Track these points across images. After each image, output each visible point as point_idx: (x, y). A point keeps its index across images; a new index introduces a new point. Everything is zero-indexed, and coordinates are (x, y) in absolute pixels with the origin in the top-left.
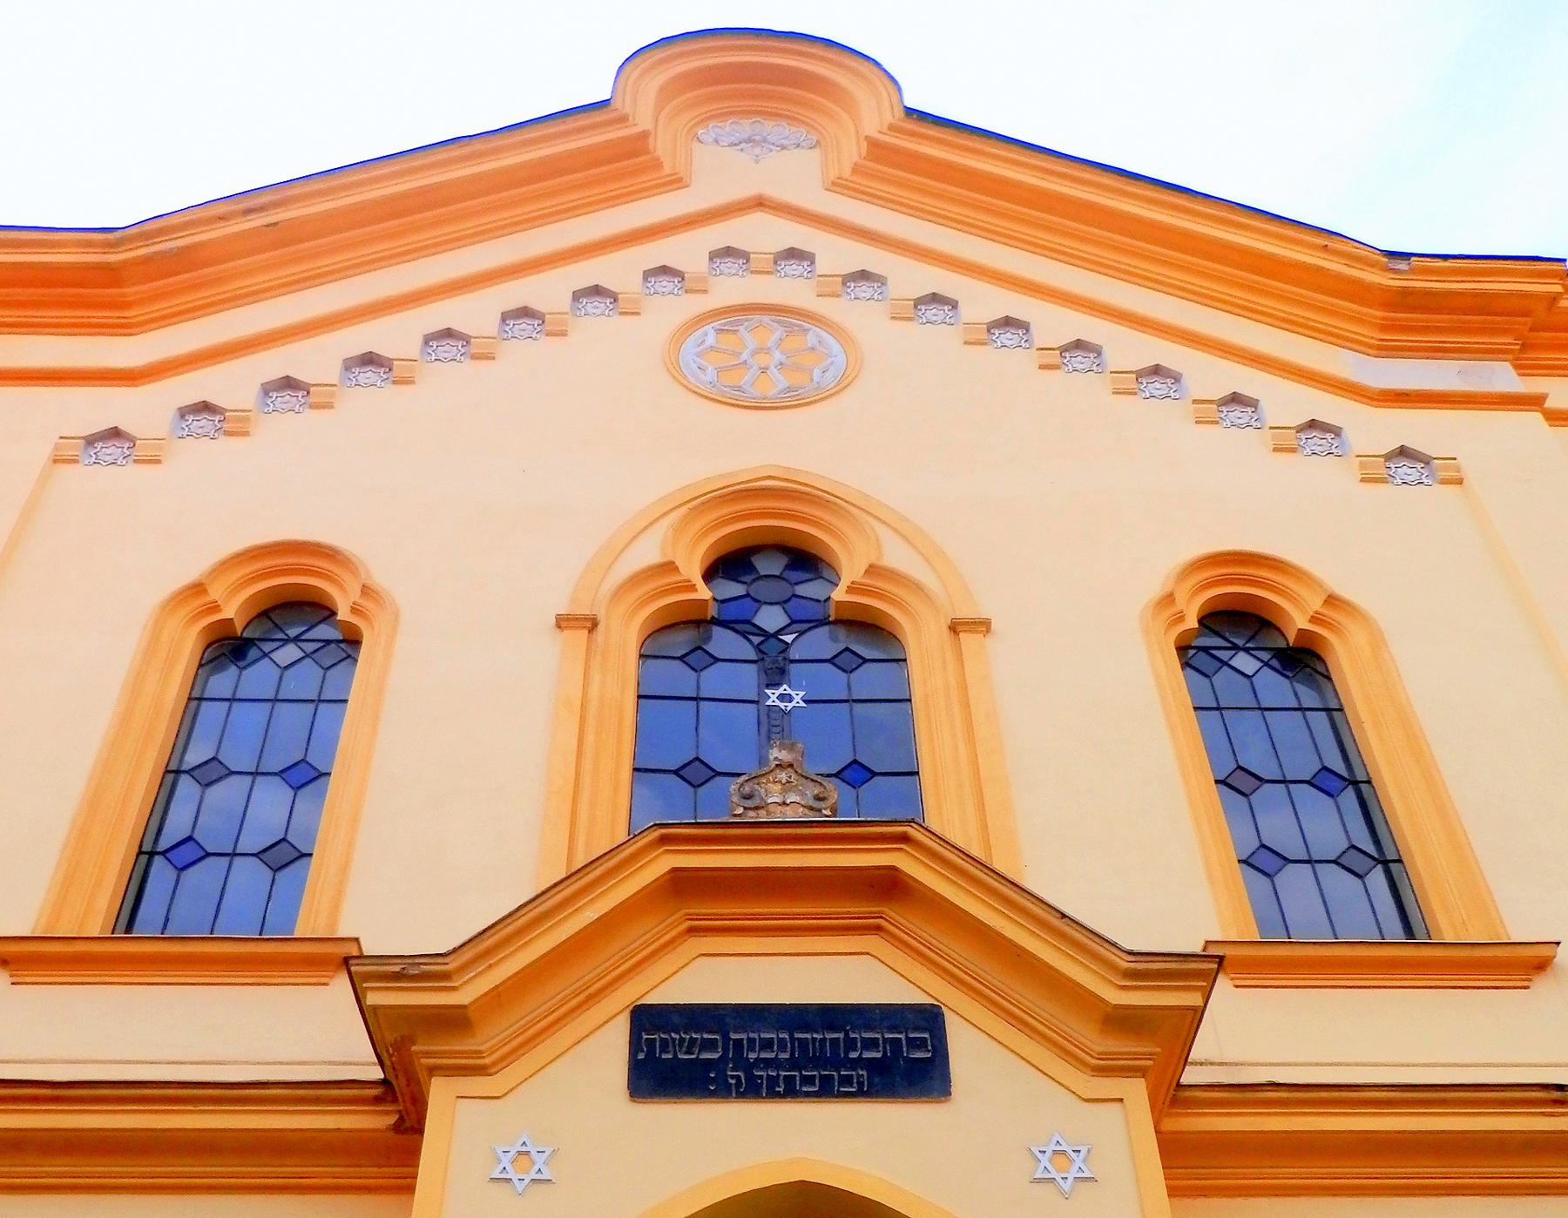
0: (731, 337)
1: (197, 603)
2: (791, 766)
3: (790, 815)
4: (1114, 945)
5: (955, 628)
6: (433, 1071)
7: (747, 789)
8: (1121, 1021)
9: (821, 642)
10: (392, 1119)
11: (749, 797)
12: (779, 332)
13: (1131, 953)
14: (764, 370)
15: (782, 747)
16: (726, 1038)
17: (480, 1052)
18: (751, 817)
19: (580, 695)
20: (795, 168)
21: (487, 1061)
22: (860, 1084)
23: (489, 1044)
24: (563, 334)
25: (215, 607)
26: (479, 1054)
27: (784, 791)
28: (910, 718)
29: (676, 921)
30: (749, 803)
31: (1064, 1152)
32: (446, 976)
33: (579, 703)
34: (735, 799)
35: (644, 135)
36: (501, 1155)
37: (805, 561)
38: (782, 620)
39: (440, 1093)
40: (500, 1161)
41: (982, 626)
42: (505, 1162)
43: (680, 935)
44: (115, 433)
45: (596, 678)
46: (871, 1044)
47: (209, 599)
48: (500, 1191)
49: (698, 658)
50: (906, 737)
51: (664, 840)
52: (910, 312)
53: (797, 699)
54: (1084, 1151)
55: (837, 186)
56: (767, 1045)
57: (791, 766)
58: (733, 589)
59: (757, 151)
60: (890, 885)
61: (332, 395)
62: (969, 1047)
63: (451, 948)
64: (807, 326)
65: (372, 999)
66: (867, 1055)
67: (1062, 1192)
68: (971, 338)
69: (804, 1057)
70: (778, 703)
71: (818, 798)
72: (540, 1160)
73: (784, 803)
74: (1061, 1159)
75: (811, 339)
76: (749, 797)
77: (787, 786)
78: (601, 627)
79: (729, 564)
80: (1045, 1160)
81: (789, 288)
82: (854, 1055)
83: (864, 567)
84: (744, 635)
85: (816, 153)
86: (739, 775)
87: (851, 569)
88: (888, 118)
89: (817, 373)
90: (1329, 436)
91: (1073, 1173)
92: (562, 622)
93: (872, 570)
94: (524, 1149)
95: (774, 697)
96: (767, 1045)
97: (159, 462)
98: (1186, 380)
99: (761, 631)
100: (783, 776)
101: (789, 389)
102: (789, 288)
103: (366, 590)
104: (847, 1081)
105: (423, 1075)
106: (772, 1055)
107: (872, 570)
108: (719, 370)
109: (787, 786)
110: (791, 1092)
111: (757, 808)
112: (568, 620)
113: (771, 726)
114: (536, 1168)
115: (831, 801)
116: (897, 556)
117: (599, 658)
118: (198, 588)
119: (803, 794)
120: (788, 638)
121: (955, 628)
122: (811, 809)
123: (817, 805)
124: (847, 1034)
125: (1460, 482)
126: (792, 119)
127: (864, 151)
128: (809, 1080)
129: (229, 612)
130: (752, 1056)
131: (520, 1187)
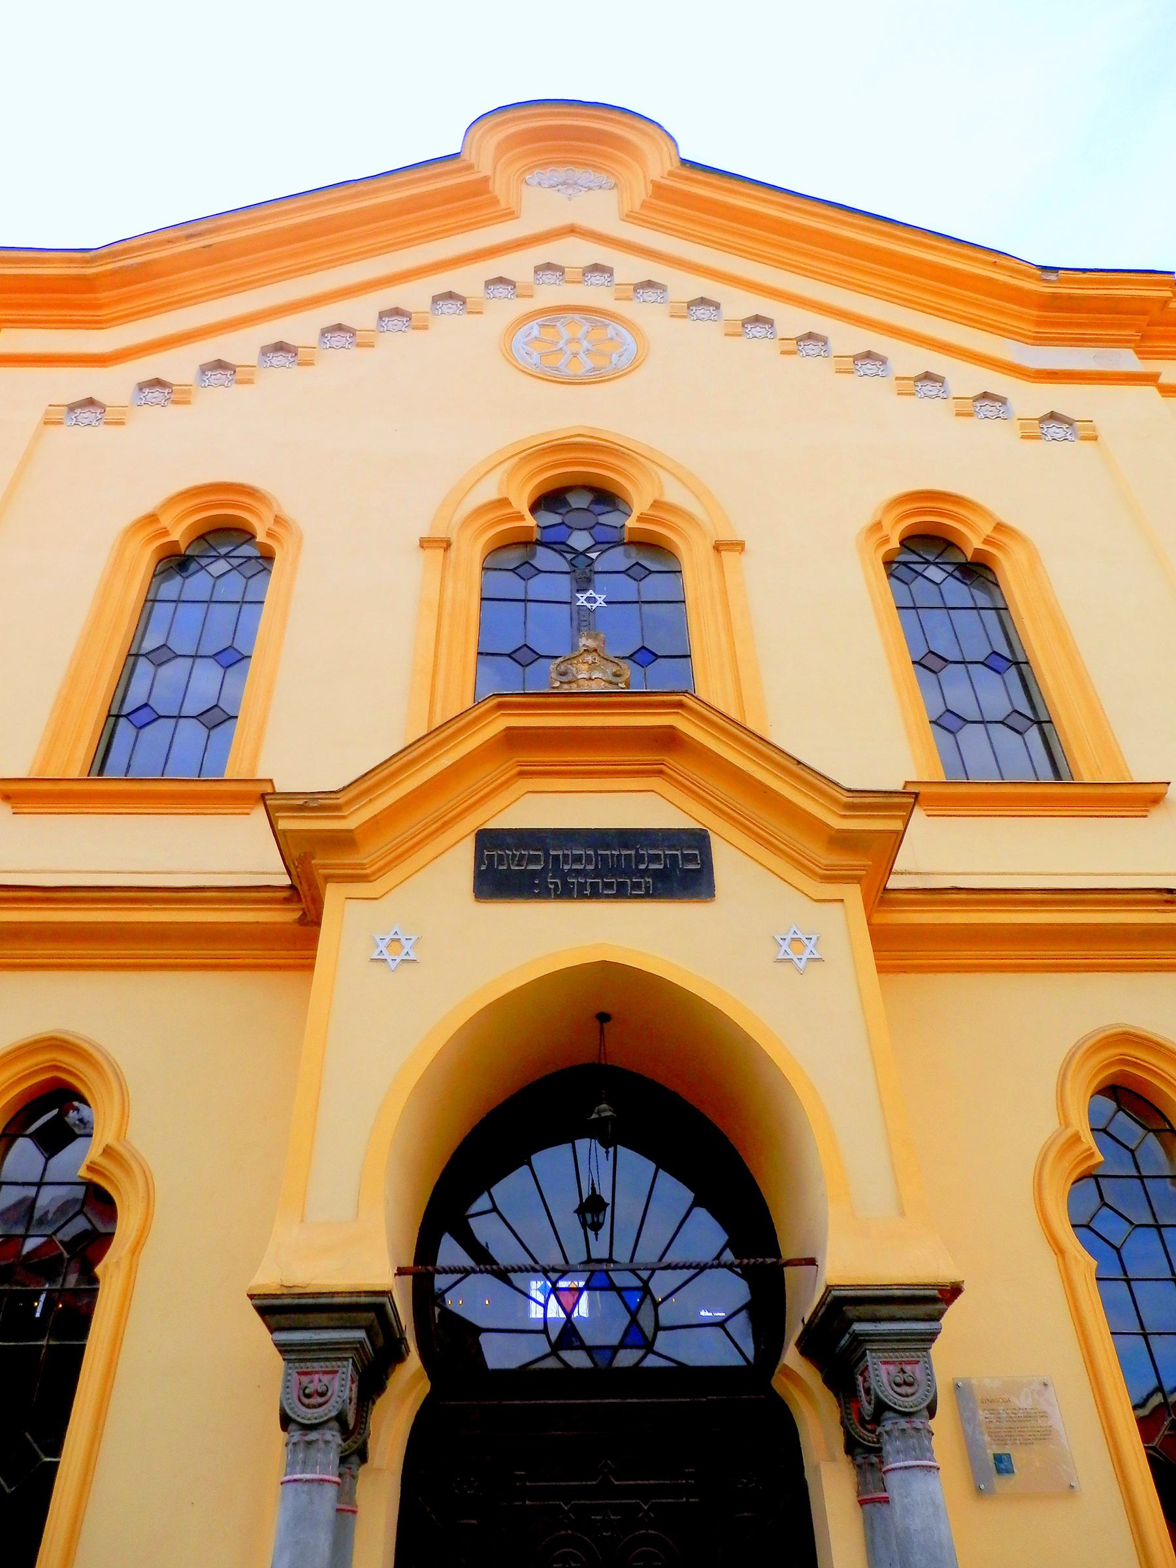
0: (551, 330)
1: (152, 529)
2: (595, 650)
3: (595, 687)
4: (837, 784)
5: (718, 548)
6: (327, 878)
7: (563, 668)
8: (842, 841)
9: (617, 558)
10: (297, 915)
11: (564, 674)
12: (587, 326)
13: (849, 791)
14: (575, 355)
15: (589, 637)
16: (547, 854)
18: (566, 688)
19: (437, 597)
20: (598, 204)
21: (368, 871)
22: (647, 888)
23: (369, 859)
24: (425, 328)
25: (165, 532)
27: (590, 670)
30: (564, 679)
31: (799, 940)
32: (337, 808)
34: (554, 675)
35: (486, 180)
37: (606, 497)
39: (333, 895)
40: (378, 946)
41: (738, 546)
42: (382, 947)
44: (90, 402)
45: (450, 585)
46: (655, 858)
47: (160, 526)
48: (378, 968)
51: (500, 706)
52: (684, 312)
53: (600, 600)
54: (814, 938)
55: (630, 217)
56: (578, 859)
57: (595, 650)
59: (570, 191)
60: (669, 740)
61: (253, 373)
62: (728, 860)
64: (607, 322)
65: (282, 825)
67: (798, 969)
68: (730, 331)
69: (605, 868)
70: (585, 603)
71: (616, 675)
72: (408, 946)
74: (796, 945)
75: (610, 332)
76: (564, 674)
77: (592, 666)
78: (454, 547)
80: (785, 945)
81: (594, 294)
82: (642, 867)
83: (650, 502)
84: (560, 553)
85: (614, 192)
87: (640, 504)
88: (668, 167)
89: (615, 357)
90: (997, 404)
91: (807, 955)
92: (425, 543)
93: (656, 504)
94: (396, 937)
95: (582, 600)
96: (578, 859)
97: (123, 423)
98: (891, 363)
99: (573, 550)
100: (589, 658)
101: (594, 369)
102: (594, 294)
103: (278, 520)
104: (637, 886)
105: (320, 881)
107: (656, 504)
108: (542, 355)
110: (595, 894)
111: (570, 682)
113: (580, 621)
115: (625, 677)
116: (674, 494)
118: (152, 518)
119: (604, 672)
121: (718, 548)
122: (611, 683)
123: (615, 680)
125: (1095, 438)
126: (596, 167)
127: (650, 193)
128: (608, 886)
129: (176, 535)
130: (566, 867)
131: (393, 965)
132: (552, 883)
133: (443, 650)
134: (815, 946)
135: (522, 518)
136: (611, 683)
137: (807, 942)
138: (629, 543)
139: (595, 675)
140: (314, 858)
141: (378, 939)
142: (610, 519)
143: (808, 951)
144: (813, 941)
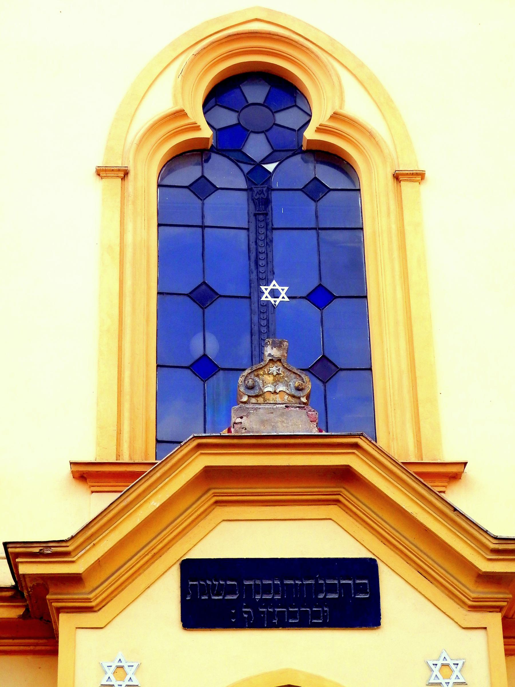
2: (279, 360)
4: (486, 532)
5: (397, 177)
6: (59, 610)
7: (250, 383)
10: (20, 612)
11: (252, 388)
13: (496, 538)
15: (274, 345)
16: (241, 584)
17: (90, 599)
19: (118, 241)
21: (93, 604)
22: (325, 618)
23: (94, 594)
26: (88, 600)
27: (276, 382)
28: (361, 242)
29: (209, 499)
30: (252, 393)
31: (448, 665)
32: (66, 554)
33: (118, 249)
34: (242, 389)
36: (107, 669)
37: (285, 90)
38: (266, 150)
39: (65, 624)
40: (106, 673)
41: (418, 176)
42: (110, 674)
43: (209, 507)
45: (129, 226)
46: (331, 589)
49: (202, 188)
50: (356, 211)
51: (200, 446)
53: (283, 294)
54: (460, 663)
56: (266, 589)
57: (279, 360)
58: (227, 118)
60: (346, 475)
62: (395, 590)
63: (70, 536)
65: (24, 569)
66: (330, 596)
69: (291, 598)
71: (298, 389)
73: (275, 392)
74: (446, 669)
76: (252, 388)
78: (131, 176)
79: (222, 93)
80: (436, 670)
82: (321, 596)
83: (329, 113)
84: (236, 162)
86: (244, 370)
87: (320, 115)
91: (453, 680)
92: (101, 172)
93: (336, 116)
94: (120, 664)
96: (266, 589)
99: (249, 160)
100: (274, 369)
104: (316, 615)
105: (53, 613)
106: (269, 597)
107: (336, 116)
109: (277, 379)
110: (282, 623)
111: (257, 396)
112: (106, 171)
113: (257, 253)
114: (128, 678)
115: (307, 391)
116: (357, 105)
117: (131, 207)
119: (287, 385)
120: (270, 167)
121: (397, 177)
122: (293, 396)
123: (297, 394)
124: (317, 581)
128: (293, 615)
130: (258, 597)
132: (246, 612)
133: (128, 300)
134: (460, 671)
135: (197, 128)
136: (293, 396)
137: (454, 667)
138: (309, 152)
139: (281, 388)
140: (47, 593)
141: (105, 665)
142: (287, 118)
143: (454, 676)
144: (459, 666)
